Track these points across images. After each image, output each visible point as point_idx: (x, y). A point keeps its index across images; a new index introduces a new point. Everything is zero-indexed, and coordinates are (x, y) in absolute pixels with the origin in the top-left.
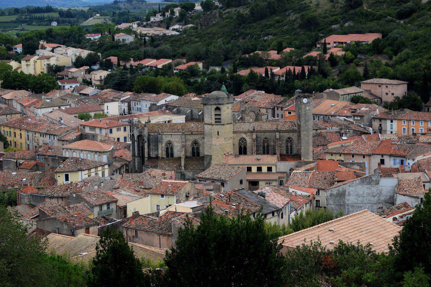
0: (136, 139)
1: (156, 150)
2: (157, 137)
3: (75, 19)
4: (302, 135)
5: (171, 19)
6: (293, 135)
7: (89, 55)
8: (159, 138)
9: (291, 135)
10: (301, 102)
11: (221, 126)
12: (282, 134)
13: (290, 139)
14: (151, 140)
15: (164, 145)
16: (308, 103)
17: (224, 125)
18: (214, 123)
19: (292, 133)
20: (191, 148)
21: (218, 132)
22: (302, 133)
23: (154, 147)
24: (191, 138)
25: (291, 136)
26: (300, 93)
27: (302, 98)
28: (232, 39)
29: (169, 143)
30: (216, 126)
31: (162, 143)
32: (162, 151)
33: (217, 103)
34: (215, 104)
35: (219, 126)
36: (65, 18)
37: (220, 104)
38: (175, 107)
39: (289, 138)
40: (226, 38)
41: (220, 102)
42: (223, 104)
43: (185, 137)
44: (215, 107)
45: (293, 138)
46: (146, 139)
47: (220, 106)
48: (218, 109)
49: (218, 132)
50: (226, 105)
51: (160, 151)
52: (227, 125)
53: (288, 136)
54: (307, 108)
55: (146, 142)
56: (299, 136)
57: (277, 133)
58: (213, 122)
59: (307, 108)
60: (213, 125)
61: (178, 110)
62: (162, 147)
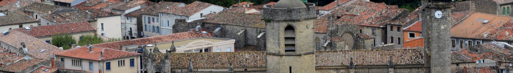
11: (296, 58)
17: (300, 55)
21: (290, 68)
27: (433, 10)
30: (287, 58)
33: (288, 18)
34: (285, 21)
35: (292, 57)
37: (294, 21)
41: (294, 17)
42: (299, 21)
44: (285, 24)
47: (294, 24)
49: (290, 68)
50: (304, 22)
54: (442, 27)
57: (390, 69)
58: (282, 50)
59: (442, 27)
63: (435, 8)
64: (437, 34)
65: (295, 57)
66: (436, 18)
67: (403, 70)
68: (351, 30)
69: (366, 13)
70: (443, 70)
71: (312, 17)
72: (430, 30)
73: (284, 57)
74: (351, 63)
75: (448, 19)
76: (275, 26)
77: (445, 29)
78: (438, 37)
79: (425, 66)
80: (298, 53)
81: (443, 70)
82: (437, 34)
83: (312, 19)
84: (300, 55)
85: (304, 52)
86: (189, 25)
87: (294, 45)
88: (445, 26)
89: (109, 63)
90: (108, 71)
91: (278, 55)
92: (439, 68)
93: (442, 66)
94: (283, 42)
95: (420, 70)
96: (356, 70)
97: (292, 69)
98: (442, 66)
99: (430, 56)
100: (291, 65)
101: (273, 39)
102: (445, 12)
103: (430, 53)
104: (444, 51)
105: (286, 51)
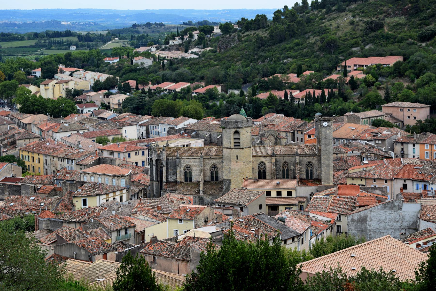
0: (154, 163)
2: (176, 162)
5: (189, 42)
7: (108, 79)
9: (311, 159)
10: (321, 126)
14: (169, 164)
15: (182, 169)
16: (328, 126)
17: (243, 149)
19: (312, 157)
20: (210, 172)
21: (237, 156)
22: (322, 157)
23: (172, 172)
24: (210, 162)
26: (320, 116)
27: (322, 122)
29: (188, 167)
30: (235, 150)
31: (180, 167)
32: (180, 175)
33: (236, 126)
34: (234, 128)
35: (238, 150)
37: (239, 128)
38: (194, 131)
39: (309, 162)
40: (245, 61)
41: (239, 126)
42: (242, 128)
43: (204, 161)
44: (234, 130)
46: (164, 163)
47: (239, 130)
48: (237, 132)
49: (237, 156)
50: (245, 129)
51: (178, 175)
52: (246, 149)
53: (308, 160)
54: (328, 132)
55: (164, 166)
56: (319, 160)
57: (297, 157)
58: (232, 145)
59: (328, 132)
61: (196, 133)
62: (180, 171)
87: (239, 143)
95: (314, 157)
100: (237, 154)
105: (234, 146)
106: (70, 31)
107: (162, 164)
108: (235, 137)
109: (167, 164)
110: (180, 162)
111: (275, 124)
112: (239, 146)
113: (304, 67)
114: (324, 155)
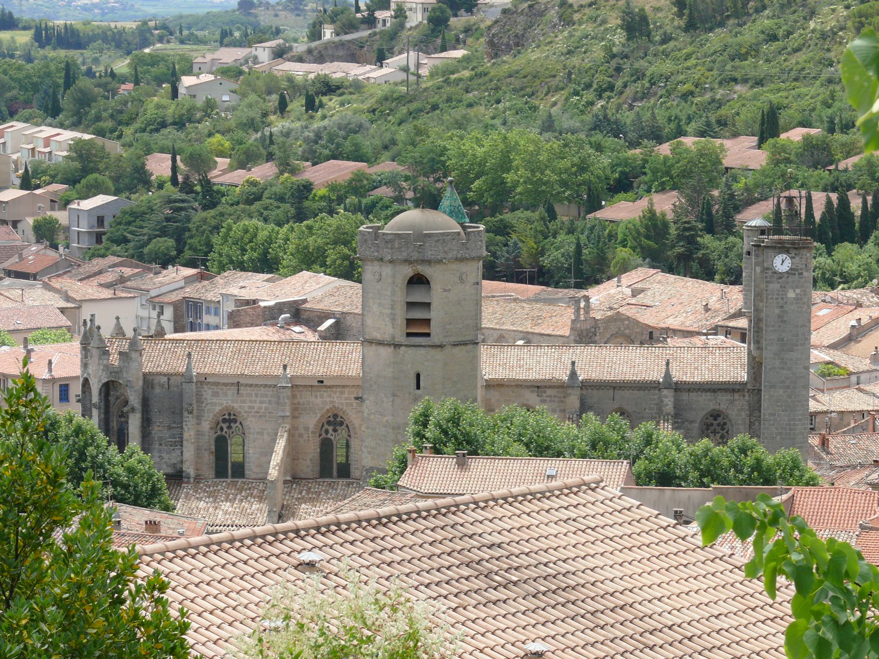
0: (95, 398)
1: (175, 444)
2: (181, 395)
3: (87, 53)
4: (764, 404)
5: (393, 35)
6: (732, 402)
7: (78, 148)
8: (186, 399)
9: (722, 402)
10: (765, 270)
11: (432, 352)
12: (685, 396)
13: (720, 420)
14: (155, 408)
15: (206, 426)
16: (792, 271)
17: (441, 346)
18: (401, 338)
19: (729, 397)
20: (318, 441)
21: (418, 376)
22: (764, 396)
23: (166, 434)
24: (318, 401)
25: (722, 407)
26: (763, 232)
27: (771, 253)
28: (600, 97)
29: (230, 419)
30: (411, 351)
31: (199, 418)
32: (198, 449)
33: (415, 255)
34: (408, 261)
35: (422, 351)
36: (54, 49)
37: (429, 262)
38: (326, 316)
39: (716, 415)
40: (576, 93)
41: (429, 254)
42: (440, 262)
43: (294, 396)
44: (408, 271)
45: (733, 413)
46: (134, 400)
47: (426, 271)
48: (418, 281)
49: (418, 376)
50: (455, 266)
51: (189, 453)
52: (456, 350)
53: (712, 406)
54: (791, 294)
55: (133, 410)
56: (755, 408)
57: (665, 392)
58: (398, 331)
59: (791, 294)
60: (397, 346)
61: (337, 324)
62: (199, 434)
63: (774, 248)
64: (777, 311)
65: (430, 349)
66: (775, 273)
67: (695, 394)
68: (627, 331)
69: (674, 301)
70: (789, 397)
71: (474, 255)
72: (762, 301)
73: (403, 348)
74: (573, 374)
75: (805, 274)
76: (384, 274)
77: (796, 299)
78: (779, 316)
79: (749, 387)
80: (435, 339)
81: (789, 397)
82: (777, 311)
83: (473, 259)
84: (441, 346)
85: (454, 339)
86: (264, 312)
87: (427, 322)
88: (798, 291)
89: (67, 385)
90: (64, 404)
91: (389, 345)
92: (781, 391)
93: (788, 387)
94: (401, 313)
95: (736, 396)
96: (584, 392)
97: (422, 378)
98: (788, 387)
99: (760, 364)
100: (420, 369)
101: (380, 305)
102: (797, 259)
103: (761, 355)
104: (792, 351)
105: (409, 335)
106: (10, 13)
107: (126, 402)
108: (412, 299)
109: (145, 403)
110: (199, 395)
111: (649, 303)
112: (428, 335)
113: (783, 117)
114: (773, 386)
